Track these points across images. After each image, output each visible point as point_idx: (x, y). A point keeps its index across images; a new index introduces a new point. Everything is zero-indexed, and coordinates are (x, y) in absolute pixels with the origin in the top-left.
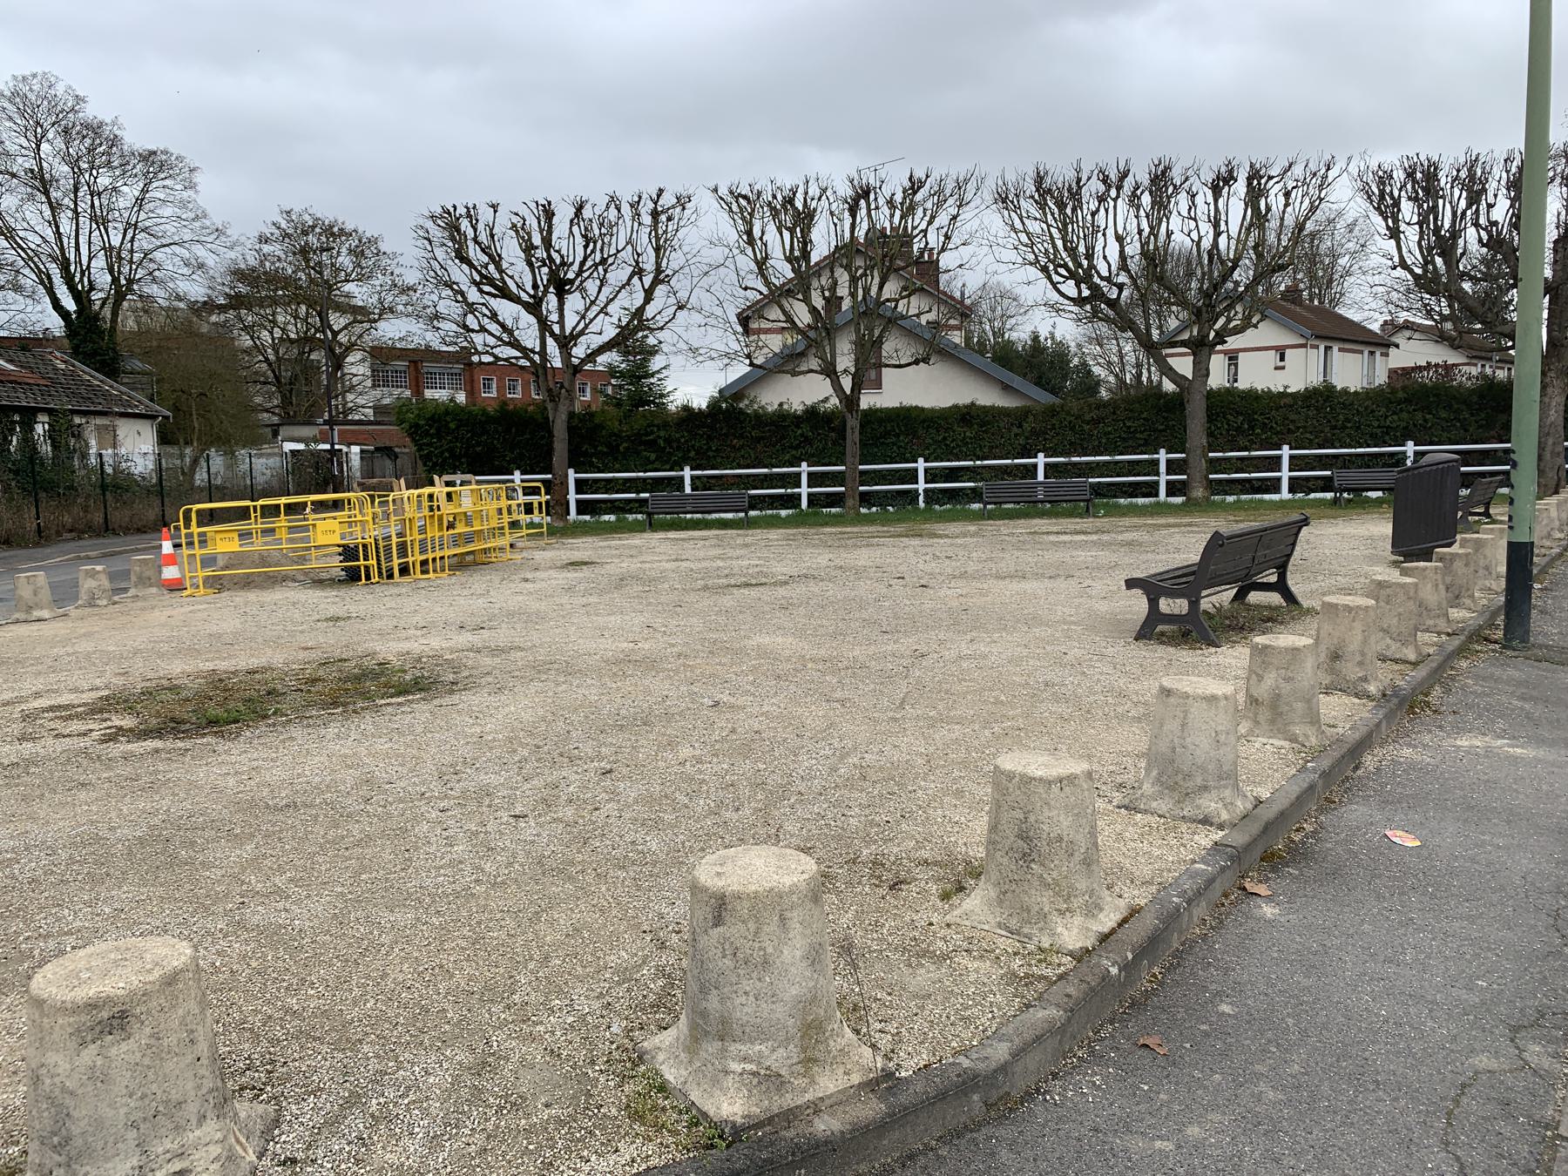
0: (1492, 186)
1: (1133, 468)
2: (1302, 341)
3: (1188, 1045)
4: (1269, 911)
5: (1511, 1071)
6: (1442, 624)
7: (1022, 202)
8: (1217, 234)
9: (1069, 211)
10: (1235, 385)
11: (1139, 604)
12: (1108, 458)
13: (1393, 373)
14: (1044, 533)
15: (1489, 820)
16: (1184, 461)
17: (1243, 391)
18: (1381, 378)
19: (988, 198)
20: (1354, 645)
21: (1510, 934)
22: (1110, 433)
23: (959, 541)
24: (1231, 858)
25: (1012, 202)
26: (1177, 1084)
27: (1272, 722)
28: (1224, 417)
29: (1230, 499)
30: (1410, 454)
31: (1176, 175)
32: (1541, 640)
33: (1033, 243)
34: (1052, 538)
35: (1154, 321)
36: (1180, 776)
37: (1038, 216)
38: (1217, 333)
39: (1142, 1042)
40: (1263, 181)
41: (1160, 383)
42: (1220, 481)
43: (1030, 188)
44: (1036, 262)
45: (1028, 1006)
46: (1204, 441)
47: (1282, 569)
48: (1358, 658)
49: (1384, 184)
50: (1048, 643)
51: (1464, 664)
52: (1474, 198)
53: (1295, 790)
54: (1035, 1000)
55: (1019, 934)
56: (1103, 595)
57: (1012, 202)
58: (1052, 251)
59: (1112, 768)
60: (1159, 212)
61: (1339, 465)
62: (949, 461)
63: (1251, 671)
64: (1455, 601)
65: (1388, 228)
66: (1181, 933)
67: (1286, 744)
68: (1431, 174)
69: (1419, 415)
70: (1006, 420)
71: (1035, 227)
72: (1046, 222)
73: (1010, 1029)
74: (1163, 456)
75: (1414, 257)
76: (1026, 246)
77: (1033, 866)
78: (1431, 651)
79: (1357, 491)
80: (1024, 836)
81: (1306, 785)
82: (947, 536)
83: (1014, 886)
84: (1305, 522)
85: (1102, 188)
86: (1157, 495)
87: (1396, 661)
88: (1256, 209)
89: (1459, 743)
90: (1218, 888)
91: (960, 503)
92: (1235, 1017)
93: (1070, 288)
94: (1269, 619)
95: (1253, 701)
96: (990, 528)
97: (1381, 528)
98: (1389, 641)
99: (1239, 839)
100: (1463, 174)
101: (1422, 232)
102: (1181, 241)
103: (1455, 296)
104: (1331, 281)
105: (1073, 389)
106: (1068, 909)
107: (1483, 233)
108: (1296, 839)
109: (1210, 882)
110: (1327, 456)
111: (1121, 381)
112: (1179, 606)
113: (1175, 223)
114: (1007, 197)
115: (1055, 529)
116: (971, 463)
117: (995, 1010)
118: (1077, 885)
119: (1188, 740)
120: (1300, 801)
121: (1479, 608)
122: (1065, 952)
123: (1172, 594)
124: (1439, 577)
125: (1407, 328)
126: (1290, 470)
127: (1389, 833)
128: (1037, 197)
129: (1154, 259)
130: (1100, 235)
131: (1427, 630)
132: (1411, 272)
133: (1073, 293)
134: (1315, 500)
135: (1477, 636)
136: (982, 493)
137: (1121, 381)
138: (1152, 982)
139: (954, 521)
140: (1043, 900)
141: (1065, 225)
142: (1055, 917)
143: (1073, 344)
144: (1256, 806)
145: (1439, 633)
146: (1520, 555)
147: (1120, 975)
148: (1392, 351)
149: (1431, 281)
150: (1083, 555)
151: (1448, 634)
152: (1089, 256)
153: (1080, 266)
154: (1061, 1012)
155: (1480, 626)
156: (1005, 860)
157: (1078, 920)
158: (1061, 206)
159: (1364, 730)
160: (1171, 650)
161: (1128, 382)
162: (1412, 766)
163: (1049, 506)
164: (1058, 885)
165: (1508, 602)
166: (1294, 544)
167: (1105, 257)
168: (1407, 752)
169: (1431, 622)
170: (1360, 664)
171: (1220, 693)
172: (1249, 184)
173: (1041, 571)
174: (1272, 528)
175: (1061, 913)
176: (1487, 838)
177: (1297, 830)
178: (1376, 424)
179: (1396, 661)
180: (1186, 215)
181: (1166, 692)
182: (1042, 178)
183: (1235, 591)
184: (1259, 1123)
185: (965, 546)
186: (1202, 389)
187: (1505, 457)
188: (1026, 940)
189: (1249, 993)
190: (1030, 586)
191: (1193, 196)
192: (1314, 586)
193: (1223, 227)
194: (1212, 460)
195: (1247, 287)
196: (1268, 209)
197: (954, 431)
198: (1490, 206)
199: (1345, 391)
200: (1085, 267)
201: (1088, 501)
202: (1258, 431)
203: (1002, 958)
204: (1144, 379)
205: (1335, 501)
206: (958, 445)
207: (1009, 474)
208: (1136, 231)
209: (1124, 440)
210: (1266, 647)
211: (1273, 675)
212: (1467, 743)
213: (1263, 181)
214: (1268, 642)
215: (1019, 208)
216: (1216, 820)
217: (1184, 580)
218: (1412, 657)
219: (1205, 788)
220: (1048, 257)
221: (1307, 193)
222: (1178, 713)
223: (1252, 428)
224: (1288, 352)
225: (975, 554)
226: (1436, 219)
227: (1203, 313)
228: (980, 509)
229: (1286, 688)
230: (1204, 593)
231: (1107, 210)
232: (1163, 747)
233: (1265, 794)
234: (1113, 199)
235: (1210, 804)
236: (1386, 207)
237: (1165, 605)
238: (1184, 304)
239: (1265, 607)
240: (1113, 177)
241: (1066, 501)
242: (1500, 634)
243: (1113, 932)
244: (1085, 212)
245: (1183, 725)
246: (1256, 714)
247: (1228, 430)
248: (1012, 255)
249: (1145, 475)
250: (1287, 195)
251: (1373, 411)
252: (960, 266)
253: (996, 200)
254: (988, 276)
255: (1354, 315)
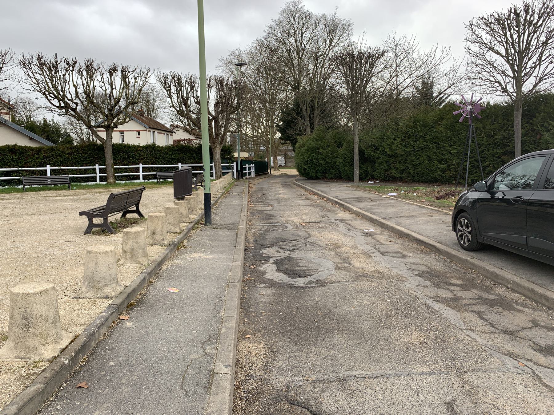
0: (197, 85)
1: (86, 171)
2: (145, 129)
3: (96, 382)
4: (129, 324)
5: (201, 357)
6: (188, 220)
7: (33, 66)
8: (112, 89)
9: (53, 73)
10: (123, 143)
11: (85, 221)
12: (76, 167)
13: (174, 141)
14: (50, 197)
15: (199, 279)
16: (105, 169)
17: (125, 145)
18: (171, 143)
19: (16, 62)
20: (159, 229)
21: (203, 314)
22: (76, 158)
23: (11, 201)
24: (115, 309)
25: (28, 66)
26: (91, 398)
27: (132, 258)
28: (119, 153)
29: (123, 182)
30: (180, 167)
31: (95, 65)
32: (215, 222)
33: (38, 83)
34: (54, 198)
35: (92, 117)
36: (96, 282)
37: (40, 73)
38: (114, 124)
39: (78, 386)
40: (127, 73)
41: (97, 142)
42: (119, 176)
43: (36, 62)
44: (40, 91)
45: (26, 387)
46: (112, 162)
47: (137, 205)
48: (161, 233)
49: (165, 80)
50: (49, 239)
51: (194, 232)
52: (192, 88)
53: (139, 280)
54: (30, 383)
55: (25, 359)
56: (73, 219)
57: (28, 66)
58: (47, 87)
59: (71, 284)
60: (90, 78)
61: (159, 170)
62: (5, 168)
63: (123, 241)
64: (192, 212)
65: (168, 94)
66: (95, 340)
67: (137, 265)
68: (179, 79)
69: (182, 155)
70: (32, 152)
71: (39, 77)
72: (44, 76)
73: (18, 399)
74: (97, 167)
75: (176, 105)
76: (36, 84)
77: (30, 329)
78: (184, 229)
79: (165, 179)
80: (25, 318)
81: (143, 278)
82: (6, 199)
83: (22, 339)
84: (144, 189)
85: (67, 66)
86: (96, 181)
87: (174, 233)
88: (125, 82)
89: (191, 256)
90: (110, 320)
91: (12, 185)
92: (115, 366)
93: (56, 102)
94: (134, 223)
95: (125, 252)
96: (26, 195)
97: (170, 190)
98: (171, 226)
99: (118, 301)
100: (188, 80)
101: (178, 97)
102: (98, 90)
103: (189, 118)
104: (153, 110)
105: (63, 142)
106: (46, 343)
107: (195, 99)
108: (139, 297)
109: (107, 319)
110: (154, 167)
111: (82, 140)
112: (100, 221)
113: (96, 83)
114: (25, 63)
115: (55, 195)
116: (17, 169)
117: (11, 393)
118: (50, 332)
119: (98, 269)
120: (141, 284)
121: (198, 214)
122: (46, 360)
123: (97, 216)
124: (186, 205)
125: (178, 127)
126: (143, 172)
127: (169, 289)
128: (39, 65)
129: (89, 95)
130: (67, 84)
131: (183, 222)
132: (176, 109)
133: (58, 105)
134: (151, 182)
135: (198, 223)
136: (22, 181)
137: (82, 140)
138: (83, 362)
139: (10, 193)
140: (36, 342)
141: (52, 78)
142: (42, 348)
143: (61, 124)
144: (125, 288)
145: (187, 223)
146: (207, 197)
147: (69, 363)
148: (174, 134)
149: (182, 112)
150: (66, 204)
151: (190, 223)
152: (63, 91)
153: (60, 94)
154: (42, 385)
155: (199, 220)
156: (17, 330)
157: (51, 346)
158: (50, 71)
159: (162, 257)
160: (98, 237)
161: (85, 140)
162: (178, 266)
163: (53, 186)
164: (42, 334)
165: (205, 211)
166: (141, 197)
167: (69, 92)
168: (176, 262)
169: (184, 220)
170: (161, 235)
171: (109, 250)
172: (122, 73)
173: (48, 211)
174: (132, 191)
175: (43, 345)
176: (198, 285)
177: (140, 294)
178: (169, 157)
179: (174, 233)
180: (100, 80)
181: (89, 252)
182: (40, 59)
183: (122, 213)
184: (121, 402)
185: (14, 203)
186: (110, 143)
187: (201, 168)
188: (28, 360)
189: (120, 356)
190: (42, 218)
191: (102, 74)
192: (149, 211)
193: (114, 87)
194: (115, 169)
195: (124, 109)
196: (129, 83)
197: (7, 156)
198: (197, 91)
199: (159, 146)
200: (62, 95)
201: (69, 184)
202: (131, 159)
203: (16, 371)
204: (91, 139)
205: (158, 182)
206: (10, 162)
207: (35, 174)
208: (81, 84)
209: (82, 161)
210: (128, 232)
211: (131, 242)
212: (193, 256)
213: (127, 73)
214: (128, 231)
215: (31, 68)
216: (110, 296)
217: (102, 211)
218: (178, 231)
219: (106, 285)
220: (46, 90)
221: (142, 79)
222: (93, 259)
223: (129, 157)
224: (141, 132)
225: (18, 206)
226: (182, 93)
227: (110, 116)
228: (22, 188)
229: (135, 246)
230: (109, 215)
231: (69, 75)
232: (89, 273)
233: (128, 283)
234: (71, 71)
235: (108, 291)
236: (167, 87)
237: (95, 221)
238: (102, 112)
239: (133, 219)
240: (71, 63)
241: (60, 184)
242: (203, 222)
243: (67, 347)
244: (60, 74)
245: (96, 264)
246: (126, 256)
247: (120, 158)
248: (30, 87)
249: (91, 174)
250: (135, 79)
251: (168, 153)
252: (5, 88)
253: (20, 64)
254: (19, 94)
255: (162, 122)
